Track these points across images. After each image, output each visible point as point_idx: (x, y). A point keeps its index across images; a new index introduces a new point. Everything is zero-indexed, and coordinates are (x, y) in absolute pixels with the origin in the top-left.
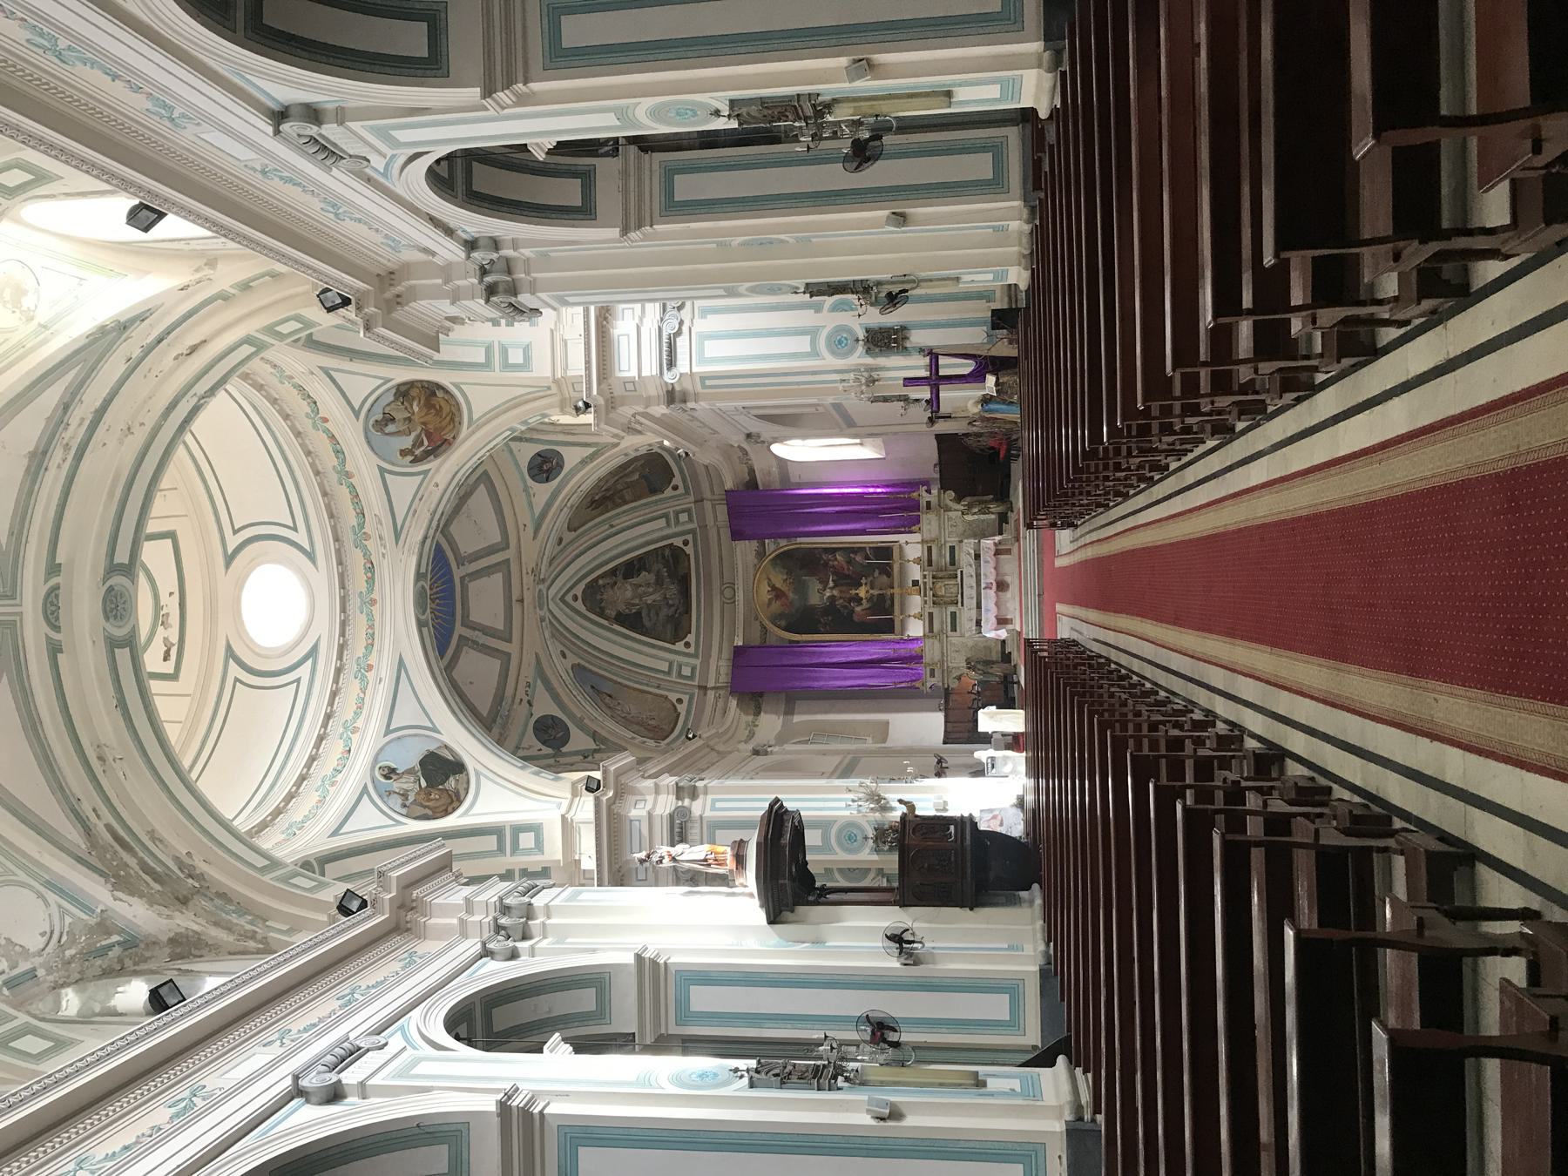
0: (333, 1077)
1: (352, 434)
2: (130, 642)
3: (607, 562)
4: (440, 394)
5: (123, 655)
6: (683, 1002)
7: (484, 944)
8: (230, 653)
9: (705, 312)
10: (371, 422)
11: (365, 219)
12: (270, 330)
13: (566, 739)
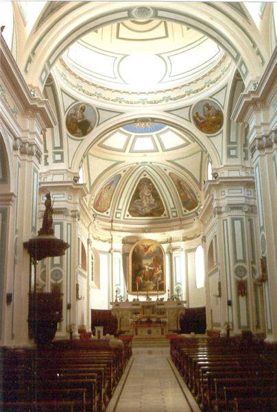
7: (20, 138)
12: (243, 62)
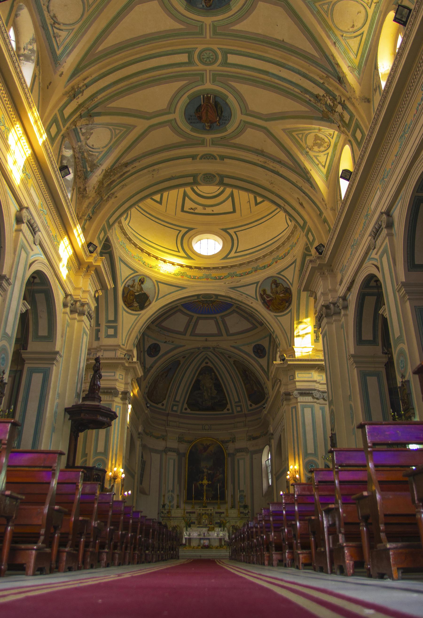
0: (25, 221)
1: (271, 272)
2: (195, 183)
3: (221, 376)
4: (287, 304)
5: (191, 180)
6: (37, 370)
7: (71, 295)
8: (190, 229)
9: (322, 409)
10: (276, 279)
11: (352, 255)
12: (309, 230)
13: (151, 355)
